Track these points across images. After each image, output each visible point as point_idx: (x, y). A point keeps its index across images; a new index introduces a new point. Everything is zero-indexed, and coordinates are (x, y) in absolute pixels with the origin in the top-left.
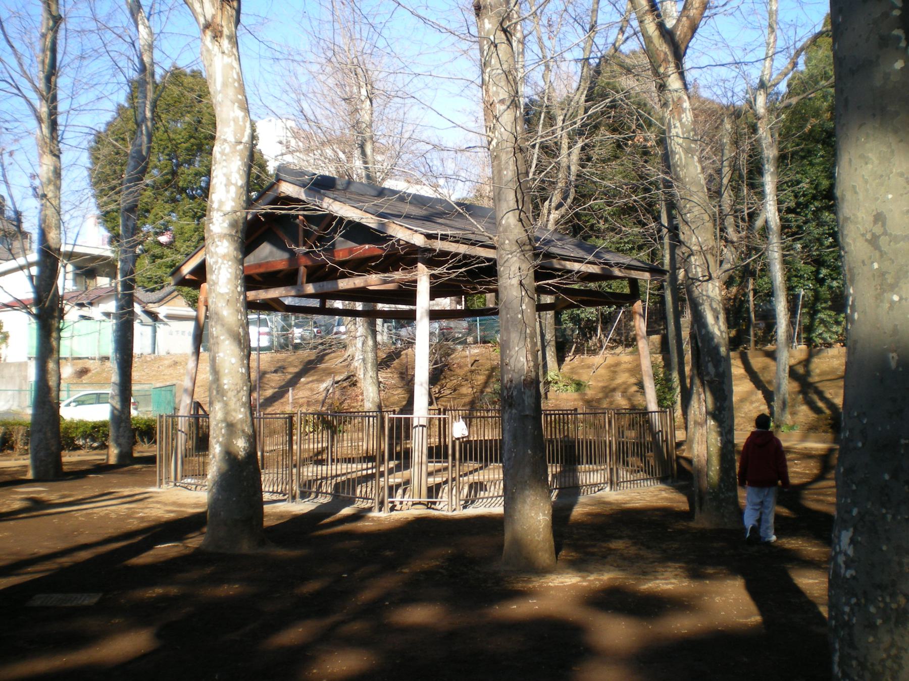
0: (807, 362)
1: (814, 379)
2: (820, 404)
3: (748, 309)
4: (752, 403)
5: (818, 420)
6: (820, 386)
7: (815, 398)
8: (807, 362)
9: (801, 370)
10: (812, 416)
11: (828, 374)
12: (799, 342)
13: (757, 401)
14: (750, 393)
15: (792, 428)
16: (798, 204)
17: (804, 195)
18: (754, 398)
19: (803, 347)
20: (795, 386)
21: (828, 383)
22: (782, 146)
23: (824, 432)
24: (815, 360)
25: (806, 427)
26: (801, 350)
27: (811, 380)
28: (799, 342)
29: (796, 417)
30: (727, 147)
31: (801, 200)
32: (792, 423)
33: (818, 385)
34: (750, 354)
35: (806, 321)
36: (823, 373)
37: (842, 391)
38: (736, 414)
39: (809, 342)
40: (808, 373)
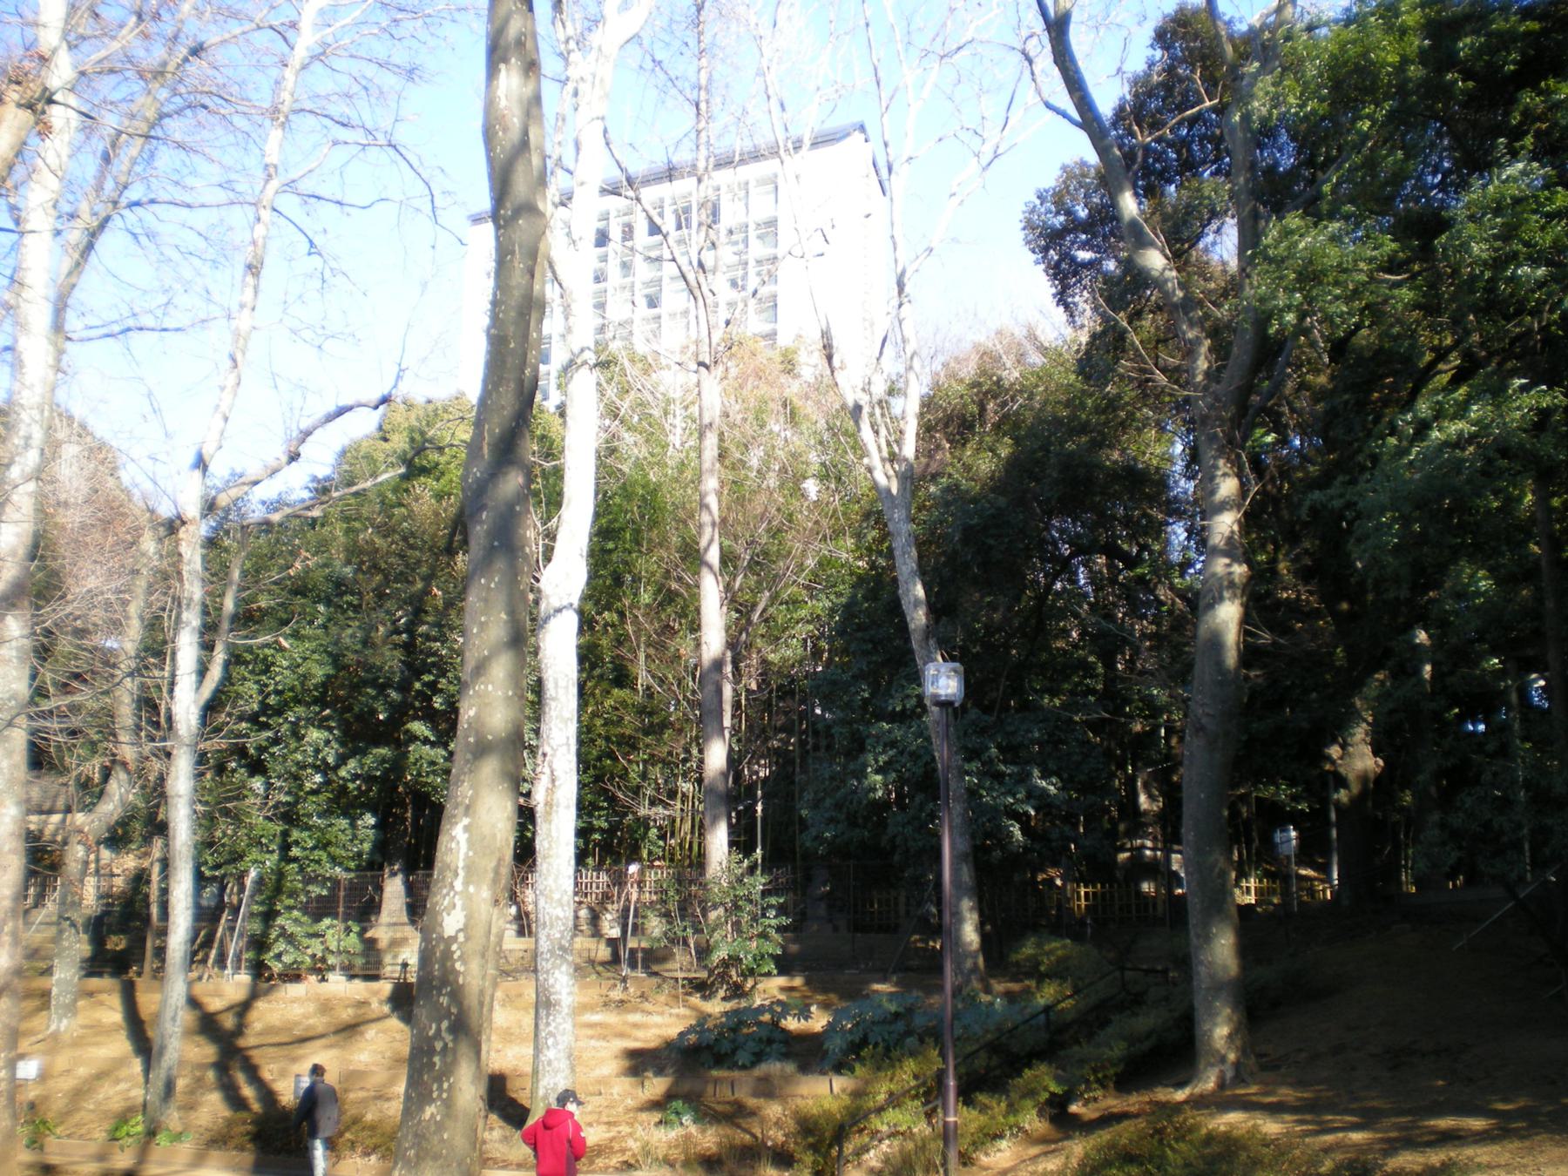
0: (243, 1008)
1: (247, 1041)
2: (248, 1092)
3: (147, 896)
4: (118, 1081)
5: (230, 1123)
6: (257, 1056)
7: (240, 1077)
8: (243, 1008)
9: (229, 1022)
10: (224, 1112)
11: (277, 1033)
12: (237, 968)
13: (130, 1078)
14: (120, 1062)
15: (178, 1137)
16: (265, 707)
17: (278, 693)
18: (124, 1073)
19: (244, 978)
20: (206, 1051)
21: (271, 1050)
22: (244, 595)
23: (236, 1148)
24: (260, 1005)
25: (207, 1136)
26: (238, 984)
27: (242, 1043)
28: (237, 968)
29: (193, 1115)
30: (1179, 467)
31: (272, 700)
32: (179, 1129)
33: (252, 1053)
34: (140, 983)
35: (256, 927)
36: (269, 1030)
37: (405, 1071)
38: (502, 1123)
39: (259, 970)
40: (240, 1030)
